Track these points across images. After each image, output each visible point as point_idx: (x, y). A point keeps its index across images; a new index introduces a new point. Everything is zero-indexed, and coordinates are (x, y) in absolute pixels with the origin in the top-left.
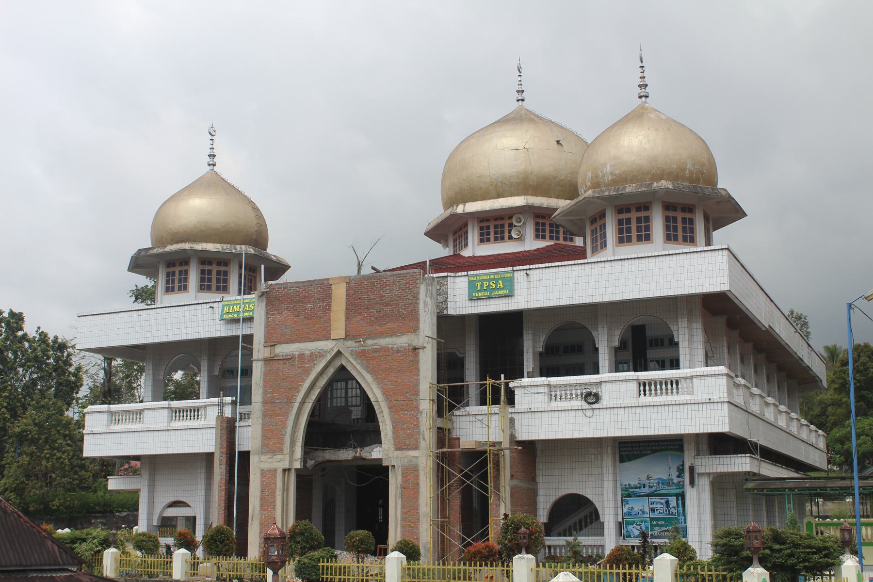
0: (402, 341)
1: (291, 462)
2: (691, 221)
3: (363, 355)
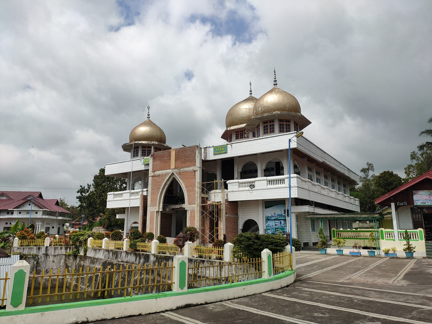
0: (191, 169)
1: (159, 209)
2: (289, 125)
3: (180, 174)
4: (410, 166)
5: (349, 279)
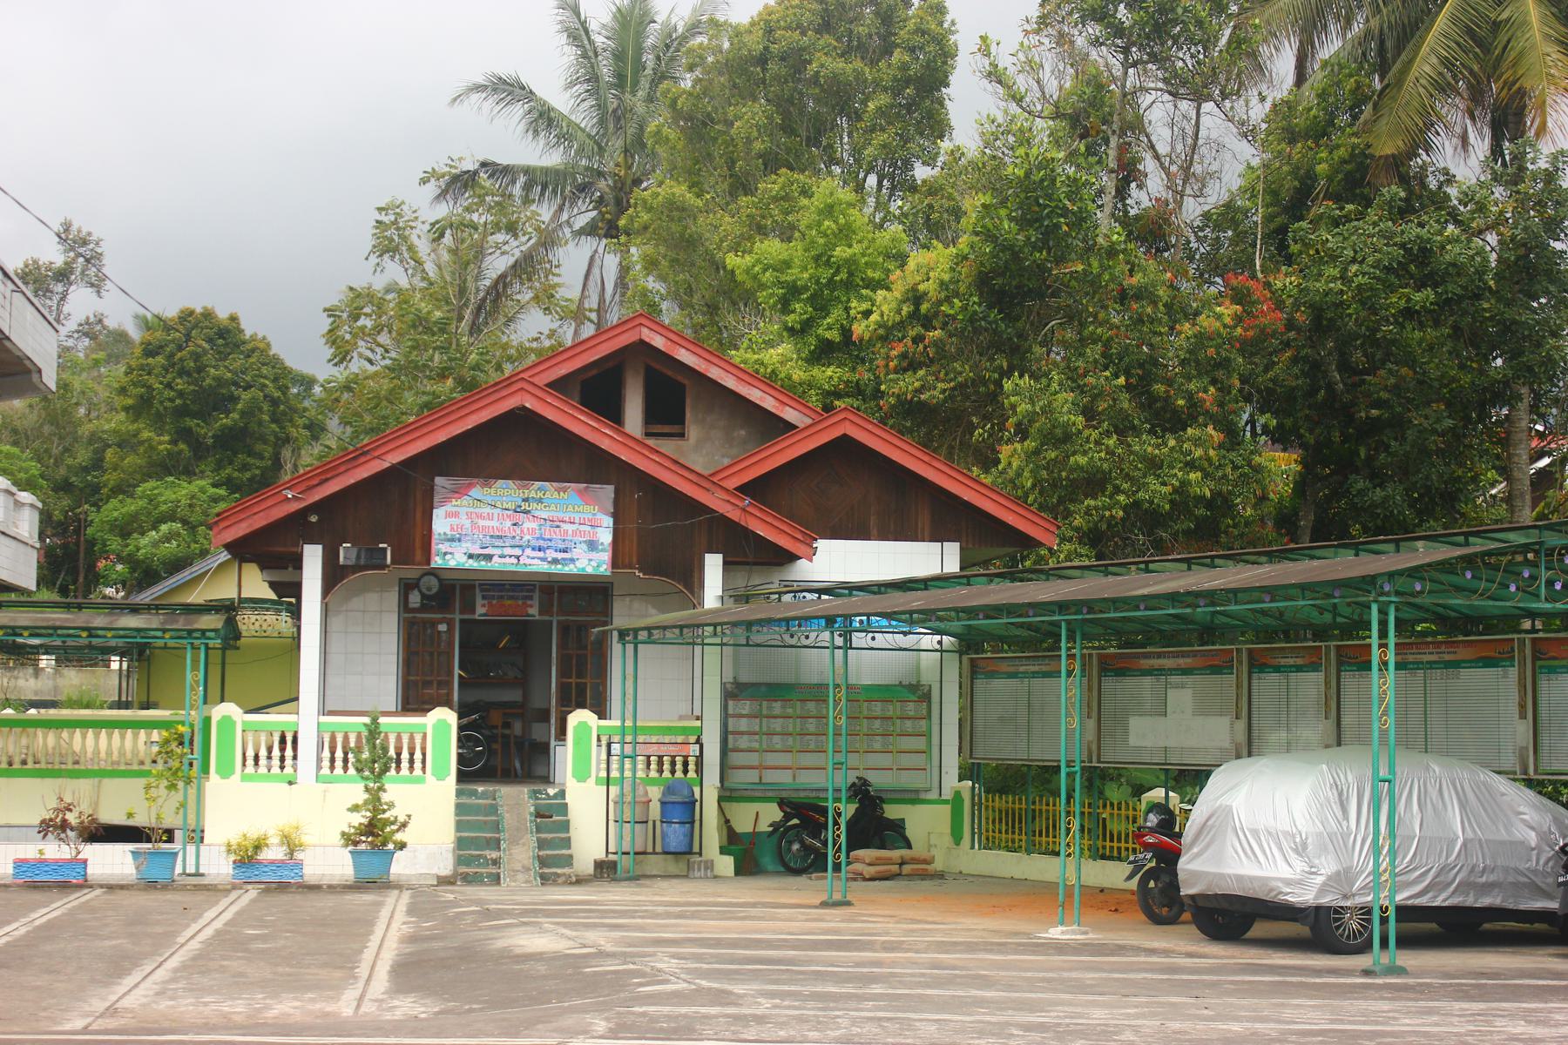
4: (359, 301)
5: (112, 1011)
